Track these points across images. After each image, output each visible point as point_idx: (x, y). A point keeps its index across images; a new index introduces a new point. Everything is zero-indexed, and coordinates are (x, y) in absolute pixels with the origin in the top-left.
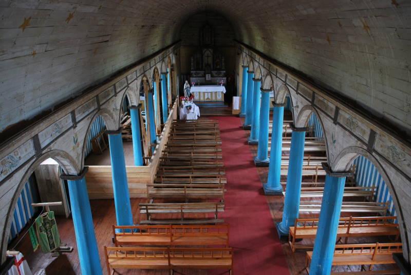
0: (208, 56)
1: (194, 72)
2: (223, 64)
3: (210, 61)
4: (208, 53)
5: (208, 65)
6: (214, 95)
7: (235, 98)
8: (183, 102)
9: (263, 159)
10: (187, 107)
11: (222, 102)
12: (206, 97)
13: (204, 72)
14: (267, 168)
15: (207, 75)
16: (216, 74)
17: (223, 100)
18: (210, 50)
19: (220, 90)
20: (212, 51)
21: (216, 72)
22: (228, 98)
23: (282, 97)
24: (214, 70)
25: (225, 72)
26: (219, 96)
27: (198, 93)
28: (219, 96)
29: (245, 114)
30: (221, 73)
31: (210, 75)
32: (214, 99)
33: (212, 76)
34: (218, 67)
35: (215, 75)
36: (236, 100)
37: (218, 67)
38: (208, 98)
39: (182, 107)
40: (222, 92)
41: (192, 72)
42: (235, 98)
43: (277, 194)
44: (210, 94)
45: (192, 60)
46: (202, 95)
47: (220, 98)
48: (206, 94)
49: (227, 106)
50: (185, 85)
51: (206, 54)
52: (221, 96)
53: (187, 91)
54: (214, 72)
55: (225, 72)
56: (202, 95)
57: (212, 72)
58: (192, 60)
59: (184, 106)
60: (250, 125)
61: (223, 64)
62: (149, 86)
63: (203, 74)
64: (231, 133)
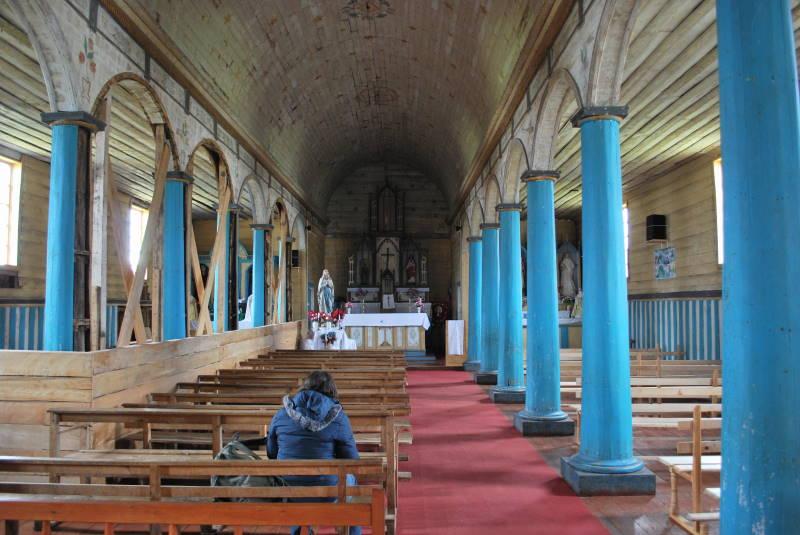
0: (388, 255)
1: (355, 290)
2: (424, 272)
3: (393, 264)
4: (388, 247)
5: (387, 273)
6: (399, 334)
7: (450, 324)
8: (315, 325)
9: (548, 411)
10: (323, 337)
11: (421, 351)
12: (380, 342)
13: (378, 289)
14: (571, 437)
15: (385, 297)
16: (408, 293)
17: (424, 347)
18: (393, 239)
19: (421, 319)
20: (397, 244)
21: (406, 290)
22: (435, 340)
23: (610, 74)
24: (401, 286)
25: (427, 290)
26: (413, 338)
27: (361, 329)
28: (413, 338)
29: (479, 361)
30: (417, 292)
31: (392, 296)
32: (400, 345)
33: (397, 300)
34: (412, 280)
35: (404, 297)
36: (455, 330)
37: (412, 280)
38: (385, 343)
39: (311, 336)
40: (421, 327)
41: (349, 289)
42: (450, 324)
43: (626, 487)
44: (389, 332)
45: (351, 262)
46: (370, 334)
47: (416, 342)
48: (381, 333)
49: (434, 358)
50: (321, 280)
51: (383, 250)
52: (417, 338)
53: (325, 295)
54: (402, 291)
55: (427, 290)
56: (370, 334)
57: (398, 289)
58: (351, 262)
59: (316, 336)
60: (495, 372)
61: (424, 272)
62: (176, 158)
63: (376, 295)
64: (449, 388)
